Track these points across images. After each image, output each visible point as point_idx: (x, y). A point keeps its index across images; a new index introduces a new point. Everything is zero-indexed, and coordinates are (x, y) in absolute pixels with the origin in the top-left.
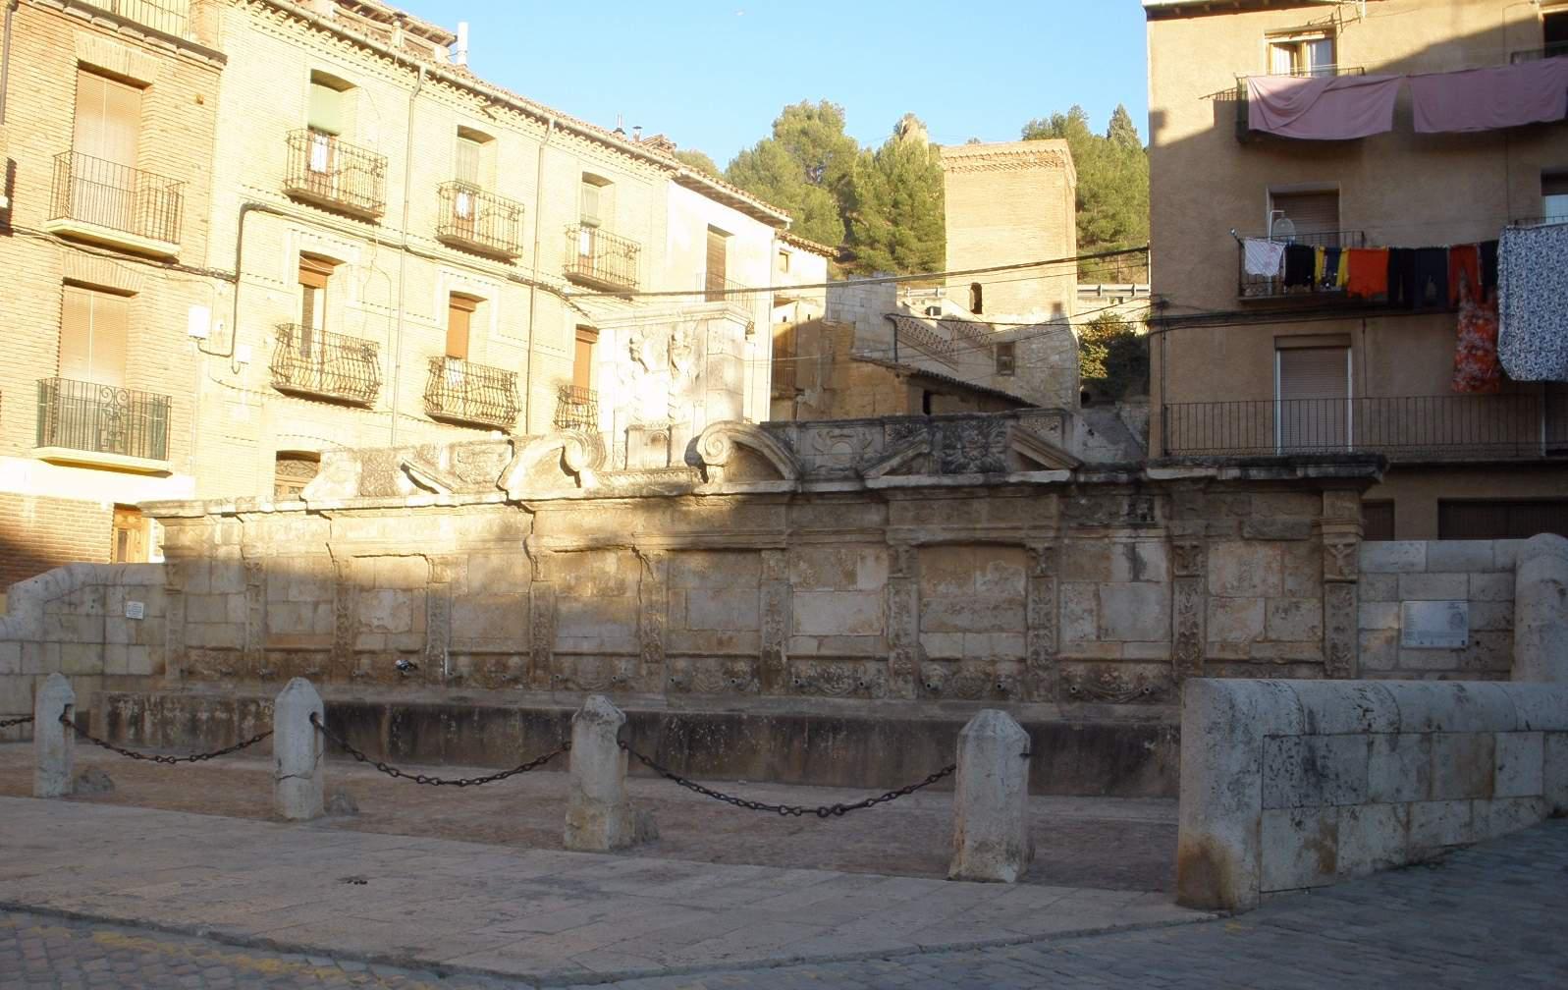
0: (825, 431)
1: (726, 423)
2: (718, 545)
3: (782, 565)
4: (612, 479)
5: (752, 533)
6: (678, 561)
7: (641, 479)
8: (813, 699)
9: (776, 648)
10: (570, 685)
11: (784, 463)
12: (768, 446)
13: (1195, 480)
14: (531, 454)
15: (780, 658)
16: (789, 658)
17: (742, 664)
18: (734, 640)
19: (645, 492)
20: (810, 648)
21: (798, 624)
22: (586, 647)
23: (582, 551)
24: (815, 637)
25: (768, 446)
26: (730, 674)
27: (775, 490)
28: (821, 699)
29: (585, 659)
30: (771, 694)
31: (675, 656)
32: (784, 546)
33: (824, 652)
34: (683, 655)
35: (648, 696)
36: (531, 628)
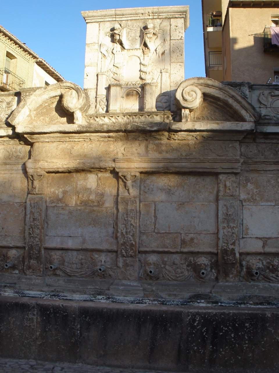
0: (266, 92)
1: (199, 79)
2: (190, 169)
3: (235, 185)
4: (97, 120)
5: (215, 161)
6: (148, 182)
7: (122, 120)
8: (261, 285)
9: (231, 247)
10: (58, 272)
11: (246, 110)
12: (233, 97)
13: (269, 159)
14: (33, 101)
15: (235, 254)
16: (241, 254)
17: (203, 258)
18: (195, 241)
19: (129, 127)
20: (257, 246)
21: (247, 229)
22: (70, 244)
23: (69, 172)
24: (260, 238)
25: (233, 97)
26: (196, 268)
27: (239, 128)
28: (267, 285)
29: (70, 253)
30: (227, 281)
31: (146, 252)
32: (239, 171)
33: (268, 250)
34: (154, 252)
35: (124, 282)
36: (27, 228)
